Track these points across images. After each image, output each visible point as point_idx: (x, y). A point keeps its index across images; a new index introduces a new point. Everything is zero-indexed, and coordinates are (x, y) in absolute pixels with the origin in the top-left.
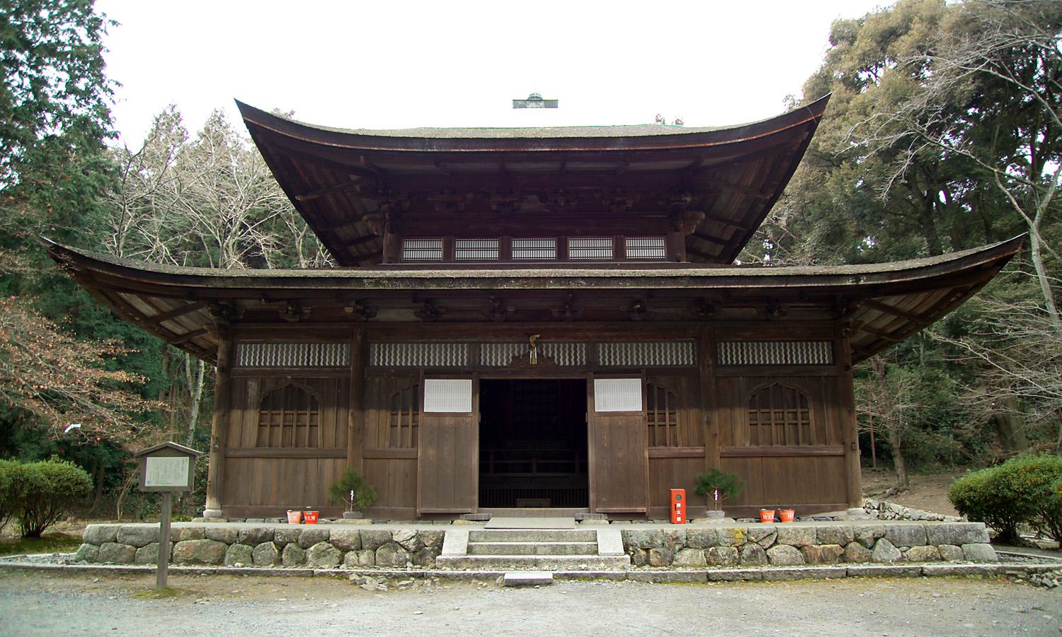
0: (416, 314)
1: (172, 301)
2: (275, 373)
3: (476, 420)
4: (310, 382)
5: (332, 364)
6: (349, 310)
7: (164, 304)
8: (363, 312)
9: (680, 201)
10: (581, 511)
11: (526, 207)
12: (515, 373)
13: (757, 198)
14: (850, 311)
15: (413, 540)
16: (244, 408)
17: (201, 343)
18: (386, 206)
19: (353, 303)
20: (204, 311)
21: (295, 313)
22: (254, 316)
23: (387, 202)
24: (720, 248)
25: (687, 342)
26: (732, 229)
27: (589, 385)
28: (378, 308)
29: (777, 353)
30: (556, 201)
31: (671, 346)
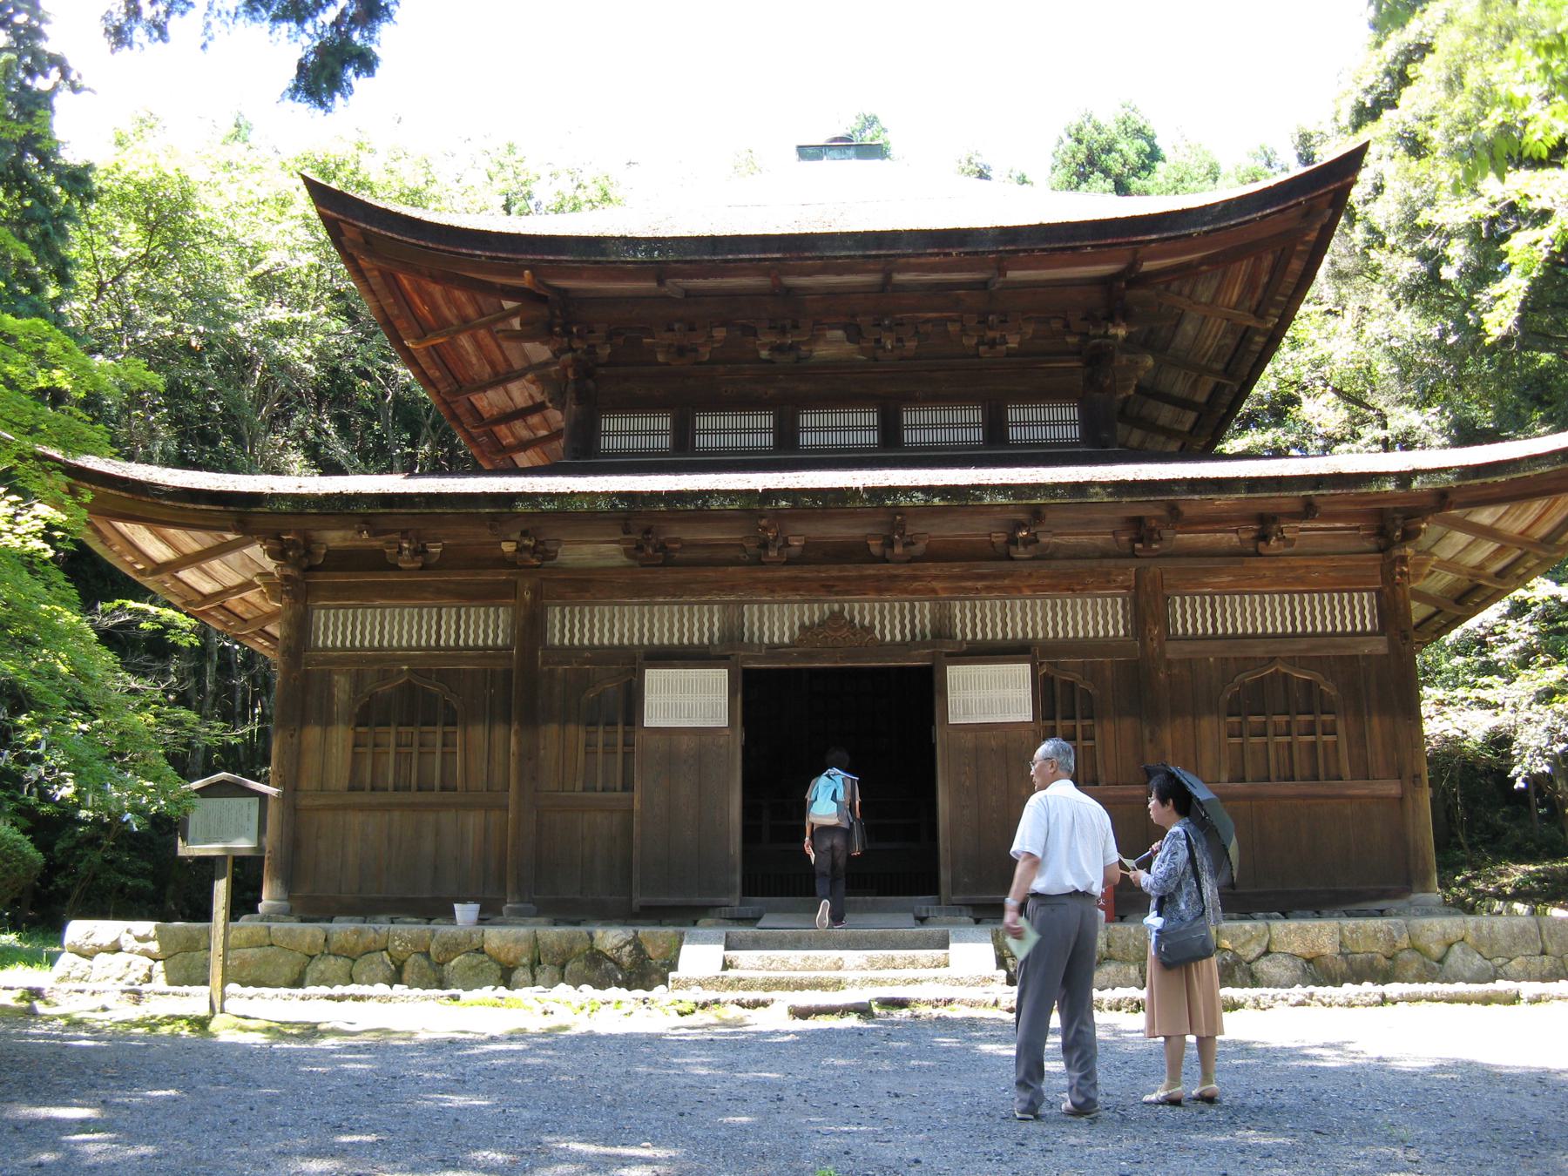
0: (627, 552)
1: (214, 534)
2: (380, 661)
3: (738, 738)
4: (442, 676)
5: (423, 643)
6: (508, 547)
7: (189, 540)
8: (534, 551)
9: (1106, 336)
10: (921, 902)
11: (822, 351)
12: (808, 656)
13: (1248, 327)
14: (1410, 535)
15: (628, 948)
16: (327, 721)
17: (239, 609)
18: (570, 355)
19: (516, 536)
20: (256, 551)
21: (416, 553)
22: (342, 560)
23: (571, 349)
24: (1190, 417)
25: (1113, 596)
26: (1210, 382)
27: (937, 677)
28: (559, 542)
29: (1089, 618)
30: (878, 341)
31: (1084, 605)
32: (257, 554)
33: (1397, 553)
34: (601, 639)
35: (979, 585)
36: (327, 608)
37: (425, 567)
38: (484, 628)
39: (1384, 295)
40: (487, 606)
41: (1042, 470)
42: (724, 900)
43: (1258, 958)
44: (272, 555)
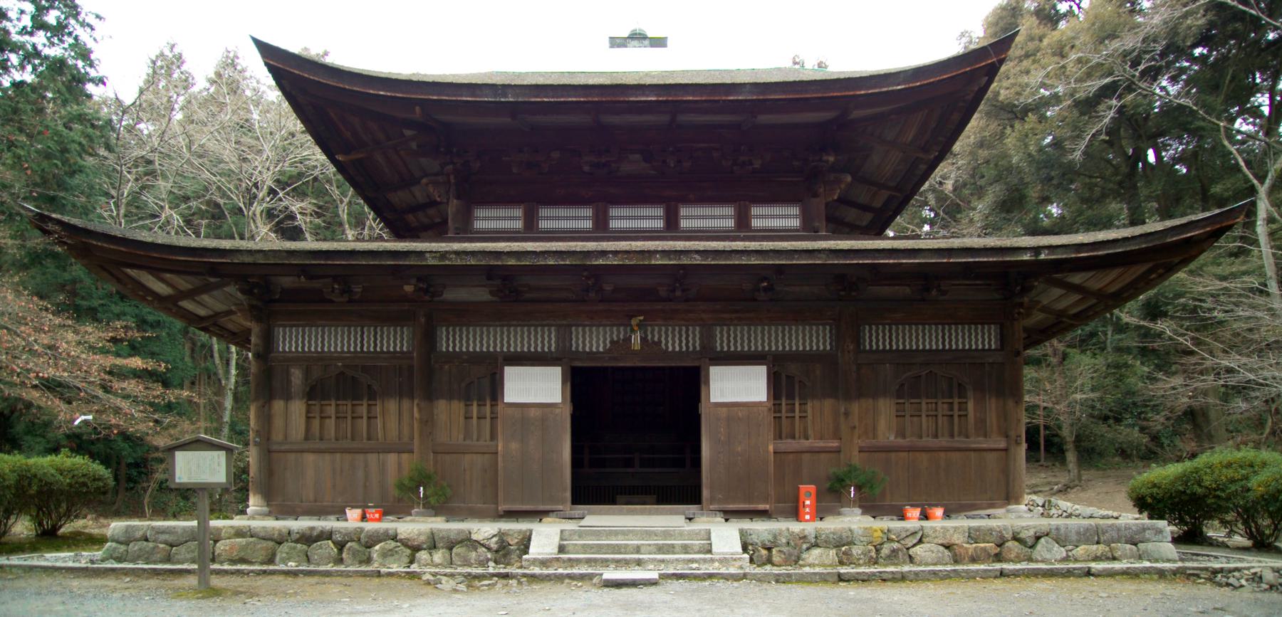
0: (491, 293)
8: (426, 291)
10: (692, 509)
11: (626, 168)
12: (615, 359)
14: (1025, 290)
15: (495, 539)
16: (288, 397)
19: (414, 281)
21: (343, 292)
22: (292, 296)
26: (885, 194)
27: (703, 373)
30: (664, 162)
32: (232, 289)
33: (1018, 300)
34: (461, 348)
35: (734, 316)
36: (284, 326)
37: (350, 301)
38: (878, 338)
39: (293, 129)
40: (396, 326)
41: (633, 243)
42: (561, 507)
43: (914, 545)
44: (243, 291)
